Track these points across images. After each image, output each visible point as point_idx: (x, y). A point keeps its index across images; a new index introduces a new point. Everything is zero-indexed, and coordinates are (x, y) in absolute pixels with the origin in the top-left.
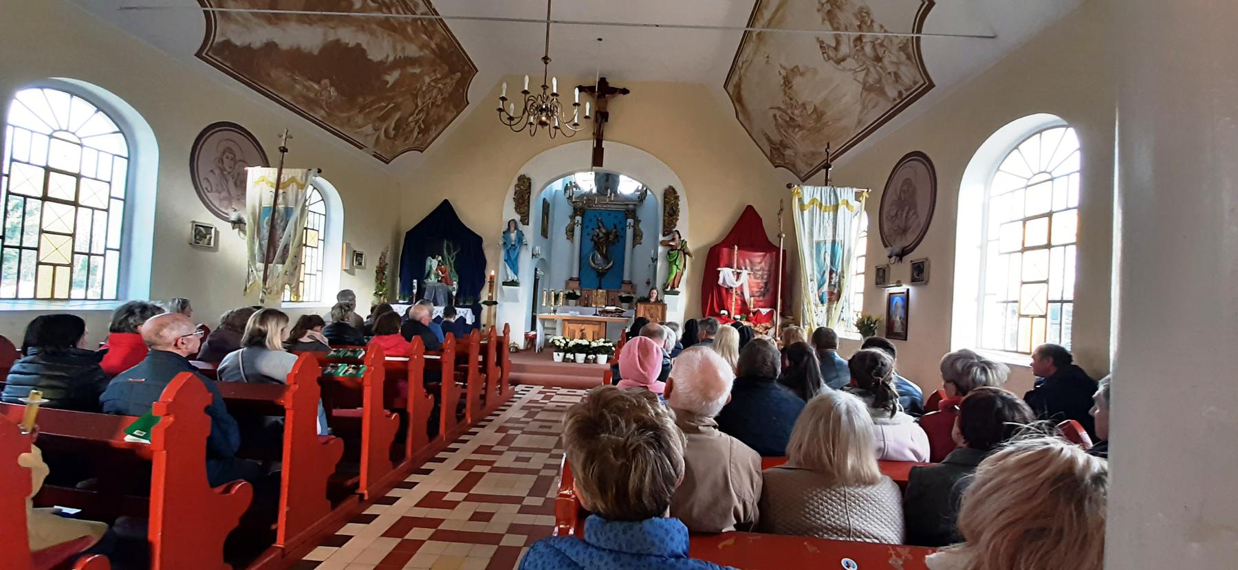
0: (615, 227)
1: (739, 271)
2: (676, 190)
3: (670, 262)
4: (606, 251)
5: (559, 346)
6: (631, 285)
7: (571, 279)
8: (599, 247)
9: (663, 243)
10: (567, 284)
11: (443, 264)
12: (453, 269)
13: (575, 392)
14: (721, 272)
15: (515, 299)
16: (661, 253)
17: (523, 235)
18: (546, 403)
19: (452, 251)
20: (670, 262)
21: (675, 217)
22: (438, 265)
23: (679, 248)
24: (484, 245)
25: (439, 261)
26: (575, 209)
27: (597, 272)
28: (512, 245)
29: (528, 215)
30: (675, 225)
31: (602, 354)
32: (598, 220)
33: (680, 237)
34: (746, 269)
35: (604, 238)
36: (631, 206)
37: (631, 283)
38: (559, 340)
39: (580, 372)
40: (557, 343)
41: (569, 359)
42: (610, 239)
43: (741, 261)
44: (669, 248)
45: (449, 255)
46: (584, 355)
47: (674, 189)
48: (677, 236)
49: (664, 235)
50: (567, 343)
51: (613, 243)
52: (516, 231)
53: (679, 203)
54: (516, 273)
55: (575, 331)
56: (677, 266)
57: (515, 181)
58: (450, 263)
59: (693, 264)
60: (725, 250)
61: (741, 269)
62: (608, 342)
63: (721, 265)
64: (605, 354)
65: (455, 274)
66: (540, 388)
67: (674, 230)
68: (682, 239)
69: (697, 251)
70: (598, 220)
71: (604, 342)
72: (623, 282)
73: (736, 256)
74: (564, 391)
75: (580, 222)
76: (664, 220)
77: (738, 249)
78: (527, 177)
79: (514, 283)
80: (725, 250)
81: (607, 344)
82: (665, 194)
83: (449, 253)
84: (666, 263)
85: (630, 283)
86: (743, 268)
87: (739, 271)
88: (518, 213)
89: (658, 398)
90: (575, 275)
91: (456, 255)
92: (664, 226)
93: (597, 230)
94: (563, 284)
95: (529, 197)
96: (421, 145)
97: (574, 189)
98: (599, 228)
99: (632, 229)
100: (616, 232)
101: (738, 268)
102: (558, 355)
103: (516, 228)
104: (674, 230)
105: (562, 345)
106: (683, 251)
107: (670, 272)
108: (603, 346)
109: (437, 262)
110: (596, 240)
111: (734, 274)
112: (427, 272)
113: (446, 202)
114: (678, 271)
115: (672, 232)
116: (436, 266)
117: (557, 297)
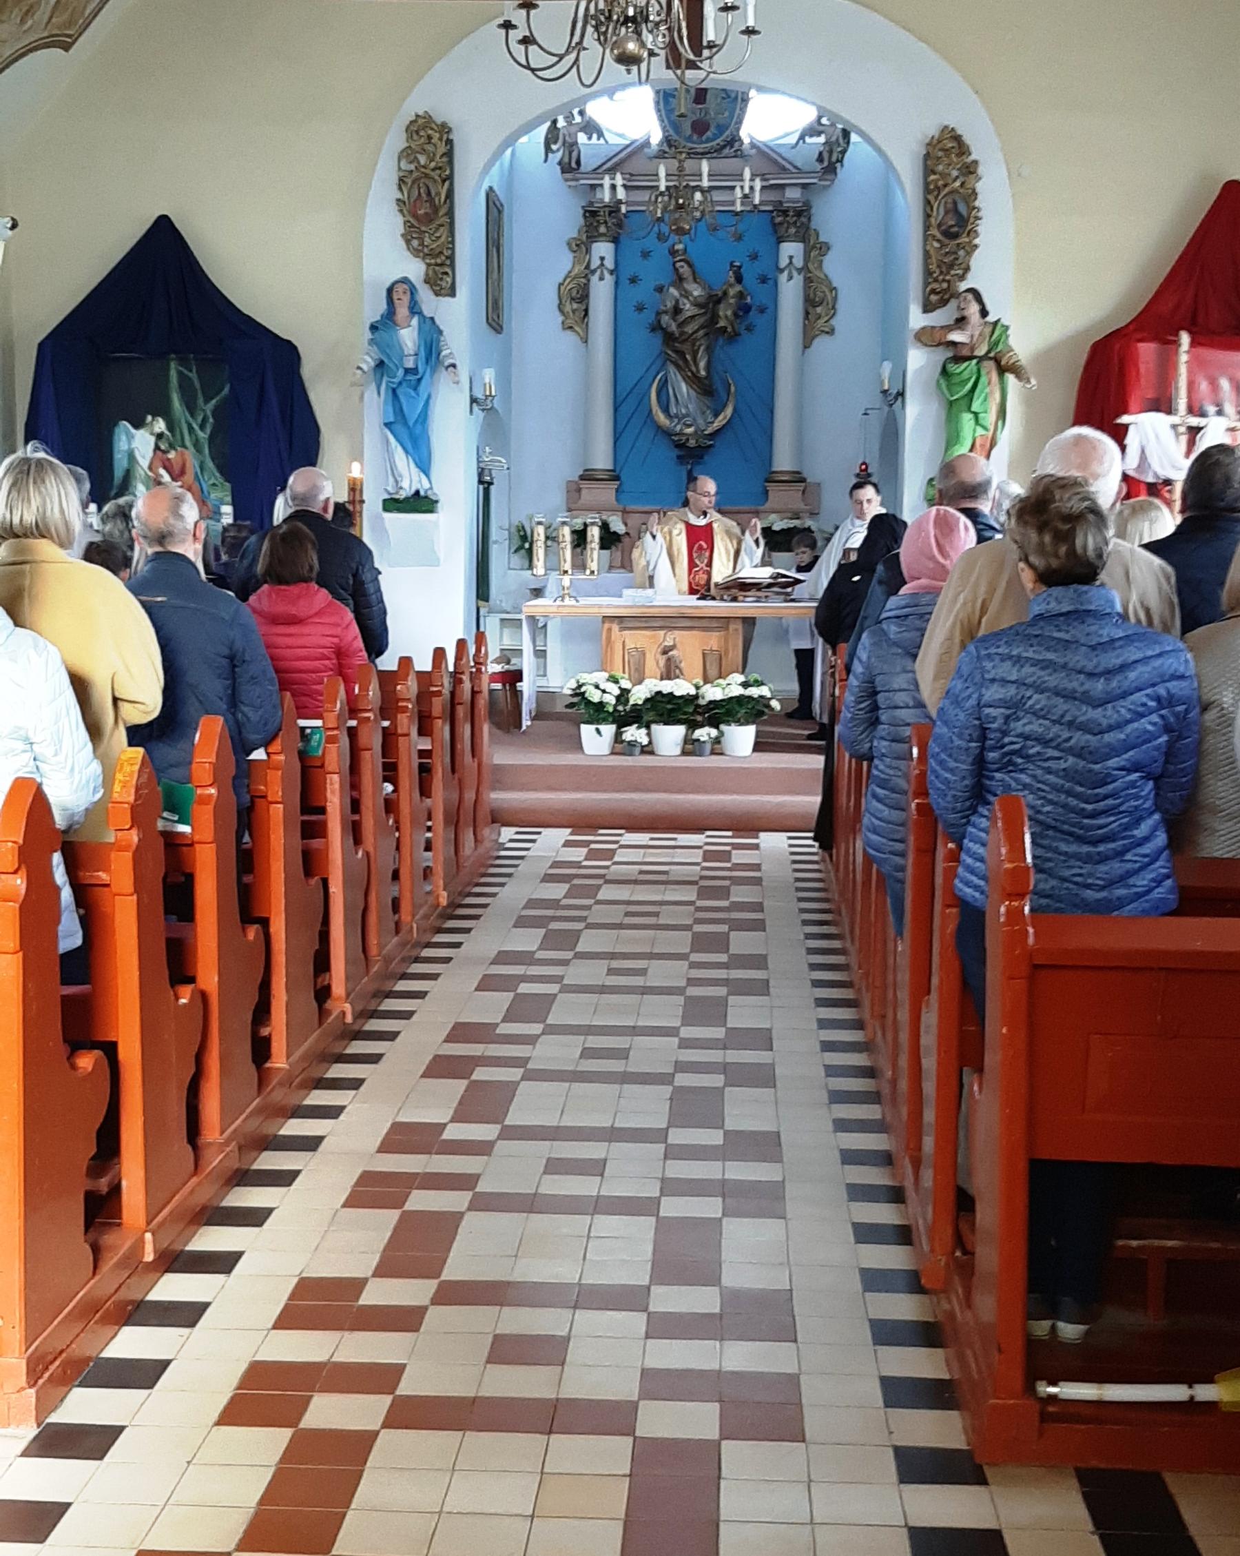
0: (739, 279)
1: (1194, 421)
2: (968, 139)
3: (951, 403)
4: (708, 367)
5: (601, 705)
6: (801, 486)
7: (588, 476)
8: (681, 354)
9: (926, 337)
10: (574, 491)
11: (172, 446)
12: (210, 464)
13: (675, 839)
14: (1131, 430)
15: (430, 559)
16: (918, 372)
17: (440, 332)
18: (607, 867)
19: (201, 400)
20: (951, 403)
21: (964, 239)
22: (157, 448)
23: (981, 351)
24: (307, 371)
25: (160, 436)
26: (591, 214)
27: (680, 446)
28: (407, 371)
29: (452, 258)
30: (967, 269)
31: (739, 722)
32: (673, 252)
33: (984, 313)
34: (1220, 413)
35: (702, 320)
36: (793, 194)
37: (803, 480)
38: (597, 687)
39: (667, 779)
40: (595, 696)
41: (632, 744)
42: (722, 323)
43: (1204, 386)
44: (942, 354)
45: (192, 415)
46: (679, 731)
47: (957, 139)
48: (974, 308)
49: (928, 308)
50: (624, 693)
51: (734, 337)
52: (415, 321)
53: (979, 187)
54: (424, 467)
55: (643, 653)
56: (976, 414)
57: (396, 140)
58: (197, 444)
59: (1029, 401)
60: (1147, 351)
61: (1203, 415)
62: (758, 683)
63: (1133, 405)
64: (747, 723)
65: (219, 478)
66: (564, 834)
67: (963, 286)
68: (991, 318)
69: (1046, 357)
70: (673, 252)
71: (745, 685)
72: (771, 478)
73: (1183, 370)
74: (642, 838)
75: (609, 263)
76: (927, 255)
77: (1194, 344)
78: (439, 121)
79: (420, 503)
80: (1147, 351)
81: (754, 692)
82: (927, 156)
83: (191, 407)
84: (934, 409)
85: (797, 478)
86: (1211, 409)
87: (1194, 421)
88: (416, 253)
89: (1041, 696)
90: (602, 460)
91: (215, 412)
92: (928, 273)
93: (673, 291)
94: (557, 498)
95: (450, 195)
96: (69, 28)
97: (582, 138)
98: (679, 280)
99: (798, 279)
100: (741, 295)
101: (1191, 410)
102: (598, 731)
103: (414, 309)
104: (963, 286)
105: (610, 700)
106: (997, 361)
107: (952, 438)
108: (742, 696)
109: (152, 439)
110: (673, 327)
111: (1177, 435)
112: (118, 473)
113: (163, 227)
114: (980, 431)
115: (956, 295)
116: (150, 454)
117: (580, 538)
